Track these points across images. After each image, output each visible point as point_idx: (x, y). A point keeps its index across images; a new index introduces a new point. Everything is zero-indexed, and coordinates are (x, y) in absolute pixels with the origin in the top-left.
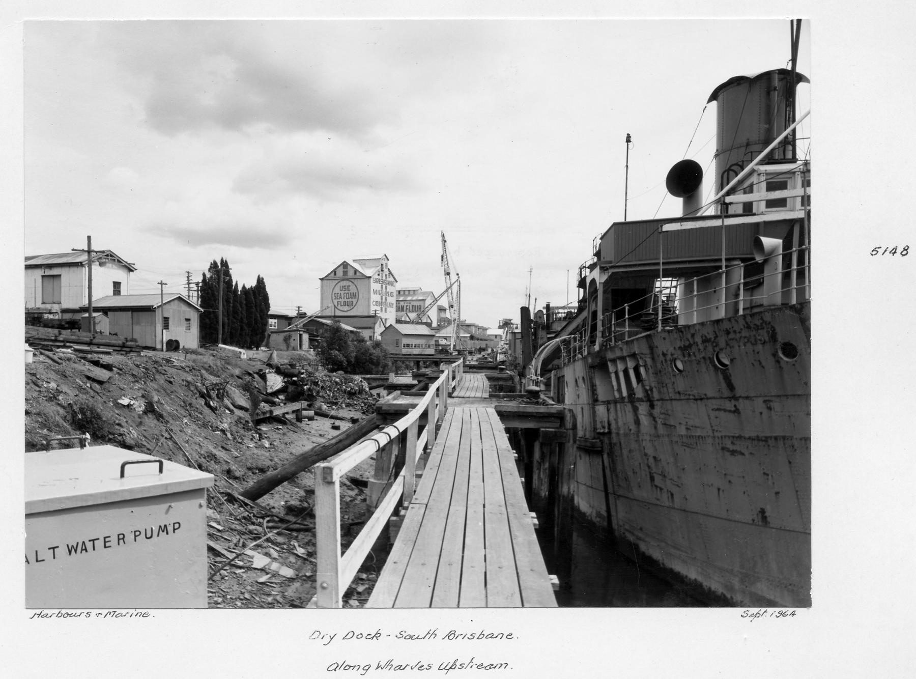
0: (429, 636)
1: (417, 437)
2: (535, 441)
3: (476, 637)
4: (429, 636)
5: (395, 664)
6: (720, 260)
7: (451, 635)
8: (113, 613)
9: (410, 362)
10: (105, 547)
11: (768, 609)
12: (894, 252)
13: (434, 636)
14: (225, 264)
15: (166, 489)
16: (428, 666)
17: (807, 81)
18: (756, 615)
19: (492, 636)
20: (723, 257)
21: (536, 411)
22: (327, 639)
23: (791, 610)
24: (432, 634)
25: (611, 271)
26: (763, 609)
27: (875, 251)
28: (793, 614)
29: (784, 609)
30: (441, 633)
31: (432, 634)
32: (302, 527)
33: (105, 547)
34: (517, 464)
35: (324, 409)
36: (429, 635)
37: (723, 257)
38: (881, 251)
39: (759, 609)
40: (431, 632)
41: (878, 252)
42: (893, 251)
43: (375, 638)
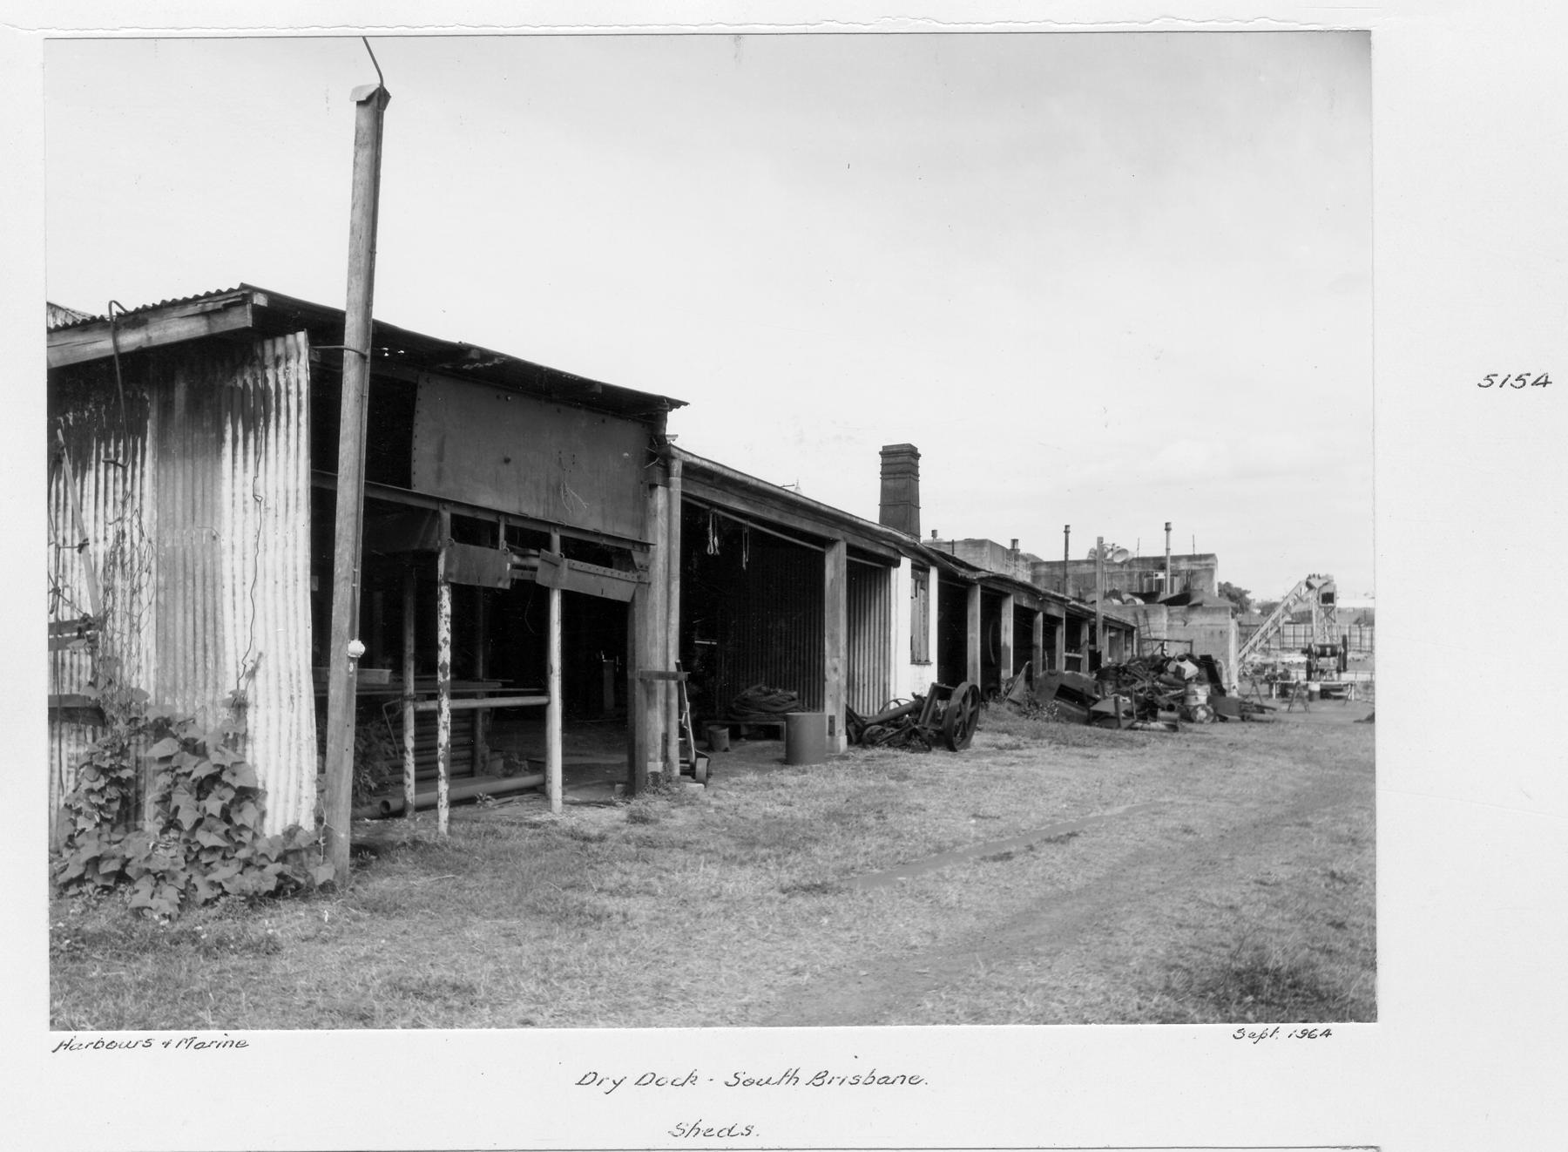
0: (786, 1079)
2: (1178, 596)
4: (786, 1079)
5: (878, 1075)
6: (454, 803)
7: (821, 1078)
10: (1191, 642)
13: (794, 1080)
15: (939, 547)
17: (677, 404)
20: (444, 813)
21: (828, 693)
22: (608, 1085)
23: (1322, 1027)
24: (791, 1077)
25: (483, 748)
26: (1272, 1026)
28: (1327, 1033)
29: (1310, 1026)
30: (805, 1076)
31: (791, 1077)
33: (1191, 642)
35: (654, 650)
36: (788, 1078)
37: (444, 813)
38: (1497, 381)
40: (791, 1074)
41: (827, 1072)
42: (1543, 380)
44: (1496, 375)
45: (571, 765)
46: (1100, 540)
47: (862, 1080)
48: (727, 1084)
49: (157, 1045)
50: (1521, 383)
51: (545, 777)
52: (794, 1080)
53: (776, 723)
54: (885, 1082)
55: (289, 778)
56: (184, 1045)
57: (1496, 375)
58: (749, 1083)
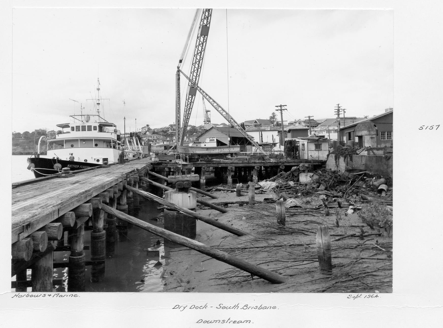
1: (190, 208)
3: (258, 308)
5: (263, 306)
8: (57, 295)
9: (329, 131)
11: (362, 294)
12: (432, 128)
13: (237, 307)
14: (16, 137)
16: (223, 321)
18: (355, 298)
19: (266, 308)
22: (182, 308)
24: (236, 306)
26: (360, 294)
27: (421, 128)
28: (377, 296)
30: (241, 306)
31: (236, 306)
32: (341, 237)
34: (12, 246)
38: (424, 128)
39: (358, 293)
40: (236, 306)
43: (204, 308)
44: (424, 126)
45: (391, 270)
46: (277, 135)
47: (258, 308)
48: (217, 308)
49: (47, 295)
50: (256, 308)
51: (116, 217)
52: (237, 307)
53: (16, 147)
54: (265, 308)
55: (373, 271)
56: (55, 296)
57: (424, 126)
58: (224, 308)
